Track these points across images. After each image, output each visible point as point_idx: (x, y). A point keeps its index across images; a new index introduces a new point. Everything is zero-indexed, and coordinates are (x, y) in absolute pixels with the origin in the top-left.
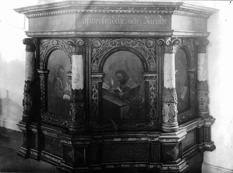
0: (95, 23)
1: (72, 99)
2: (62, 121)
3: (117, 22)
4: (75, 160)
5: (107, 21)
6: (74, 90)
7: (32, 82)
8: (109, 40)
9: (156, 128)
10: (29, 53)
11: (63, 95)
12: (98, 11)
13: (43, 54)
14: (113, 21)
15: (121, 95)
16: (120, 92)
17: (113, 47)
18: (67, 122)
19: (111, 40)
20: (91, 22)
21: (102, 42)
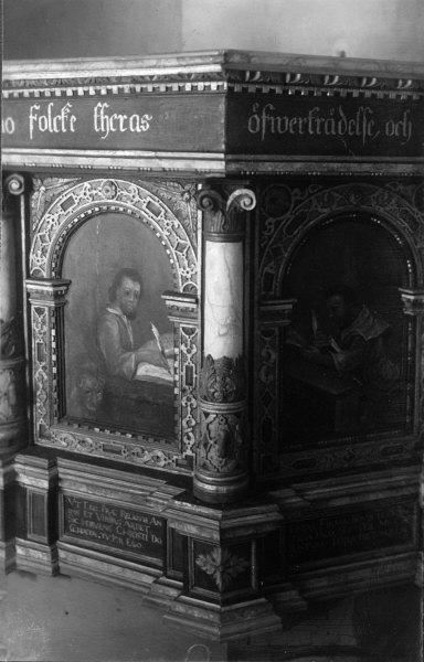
0: (47, 130)
1: (212, 390)
2: (139, 450)
3: (354, 129)
4: (223, 581)
5: (322, 125)
6: (218, 360)
7: (241, 360)
8: (313, 189)
9: (209, 407)
10: (230, 246)
11: (136, 366)
12: (274, 91)
13: (49, 227)
14: (340, 127)
15: (339, 363)
16: (335, 352)
17: (325, 210)
18: (160, 454)
19: (321, 187)
20: (276, 129)
21: (292, 194)
